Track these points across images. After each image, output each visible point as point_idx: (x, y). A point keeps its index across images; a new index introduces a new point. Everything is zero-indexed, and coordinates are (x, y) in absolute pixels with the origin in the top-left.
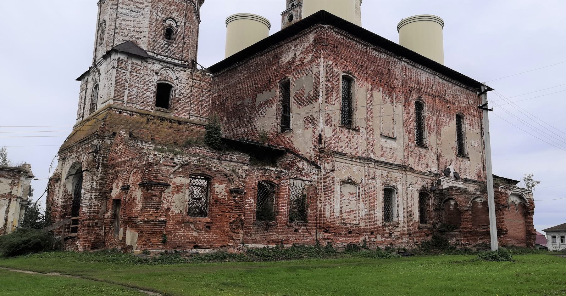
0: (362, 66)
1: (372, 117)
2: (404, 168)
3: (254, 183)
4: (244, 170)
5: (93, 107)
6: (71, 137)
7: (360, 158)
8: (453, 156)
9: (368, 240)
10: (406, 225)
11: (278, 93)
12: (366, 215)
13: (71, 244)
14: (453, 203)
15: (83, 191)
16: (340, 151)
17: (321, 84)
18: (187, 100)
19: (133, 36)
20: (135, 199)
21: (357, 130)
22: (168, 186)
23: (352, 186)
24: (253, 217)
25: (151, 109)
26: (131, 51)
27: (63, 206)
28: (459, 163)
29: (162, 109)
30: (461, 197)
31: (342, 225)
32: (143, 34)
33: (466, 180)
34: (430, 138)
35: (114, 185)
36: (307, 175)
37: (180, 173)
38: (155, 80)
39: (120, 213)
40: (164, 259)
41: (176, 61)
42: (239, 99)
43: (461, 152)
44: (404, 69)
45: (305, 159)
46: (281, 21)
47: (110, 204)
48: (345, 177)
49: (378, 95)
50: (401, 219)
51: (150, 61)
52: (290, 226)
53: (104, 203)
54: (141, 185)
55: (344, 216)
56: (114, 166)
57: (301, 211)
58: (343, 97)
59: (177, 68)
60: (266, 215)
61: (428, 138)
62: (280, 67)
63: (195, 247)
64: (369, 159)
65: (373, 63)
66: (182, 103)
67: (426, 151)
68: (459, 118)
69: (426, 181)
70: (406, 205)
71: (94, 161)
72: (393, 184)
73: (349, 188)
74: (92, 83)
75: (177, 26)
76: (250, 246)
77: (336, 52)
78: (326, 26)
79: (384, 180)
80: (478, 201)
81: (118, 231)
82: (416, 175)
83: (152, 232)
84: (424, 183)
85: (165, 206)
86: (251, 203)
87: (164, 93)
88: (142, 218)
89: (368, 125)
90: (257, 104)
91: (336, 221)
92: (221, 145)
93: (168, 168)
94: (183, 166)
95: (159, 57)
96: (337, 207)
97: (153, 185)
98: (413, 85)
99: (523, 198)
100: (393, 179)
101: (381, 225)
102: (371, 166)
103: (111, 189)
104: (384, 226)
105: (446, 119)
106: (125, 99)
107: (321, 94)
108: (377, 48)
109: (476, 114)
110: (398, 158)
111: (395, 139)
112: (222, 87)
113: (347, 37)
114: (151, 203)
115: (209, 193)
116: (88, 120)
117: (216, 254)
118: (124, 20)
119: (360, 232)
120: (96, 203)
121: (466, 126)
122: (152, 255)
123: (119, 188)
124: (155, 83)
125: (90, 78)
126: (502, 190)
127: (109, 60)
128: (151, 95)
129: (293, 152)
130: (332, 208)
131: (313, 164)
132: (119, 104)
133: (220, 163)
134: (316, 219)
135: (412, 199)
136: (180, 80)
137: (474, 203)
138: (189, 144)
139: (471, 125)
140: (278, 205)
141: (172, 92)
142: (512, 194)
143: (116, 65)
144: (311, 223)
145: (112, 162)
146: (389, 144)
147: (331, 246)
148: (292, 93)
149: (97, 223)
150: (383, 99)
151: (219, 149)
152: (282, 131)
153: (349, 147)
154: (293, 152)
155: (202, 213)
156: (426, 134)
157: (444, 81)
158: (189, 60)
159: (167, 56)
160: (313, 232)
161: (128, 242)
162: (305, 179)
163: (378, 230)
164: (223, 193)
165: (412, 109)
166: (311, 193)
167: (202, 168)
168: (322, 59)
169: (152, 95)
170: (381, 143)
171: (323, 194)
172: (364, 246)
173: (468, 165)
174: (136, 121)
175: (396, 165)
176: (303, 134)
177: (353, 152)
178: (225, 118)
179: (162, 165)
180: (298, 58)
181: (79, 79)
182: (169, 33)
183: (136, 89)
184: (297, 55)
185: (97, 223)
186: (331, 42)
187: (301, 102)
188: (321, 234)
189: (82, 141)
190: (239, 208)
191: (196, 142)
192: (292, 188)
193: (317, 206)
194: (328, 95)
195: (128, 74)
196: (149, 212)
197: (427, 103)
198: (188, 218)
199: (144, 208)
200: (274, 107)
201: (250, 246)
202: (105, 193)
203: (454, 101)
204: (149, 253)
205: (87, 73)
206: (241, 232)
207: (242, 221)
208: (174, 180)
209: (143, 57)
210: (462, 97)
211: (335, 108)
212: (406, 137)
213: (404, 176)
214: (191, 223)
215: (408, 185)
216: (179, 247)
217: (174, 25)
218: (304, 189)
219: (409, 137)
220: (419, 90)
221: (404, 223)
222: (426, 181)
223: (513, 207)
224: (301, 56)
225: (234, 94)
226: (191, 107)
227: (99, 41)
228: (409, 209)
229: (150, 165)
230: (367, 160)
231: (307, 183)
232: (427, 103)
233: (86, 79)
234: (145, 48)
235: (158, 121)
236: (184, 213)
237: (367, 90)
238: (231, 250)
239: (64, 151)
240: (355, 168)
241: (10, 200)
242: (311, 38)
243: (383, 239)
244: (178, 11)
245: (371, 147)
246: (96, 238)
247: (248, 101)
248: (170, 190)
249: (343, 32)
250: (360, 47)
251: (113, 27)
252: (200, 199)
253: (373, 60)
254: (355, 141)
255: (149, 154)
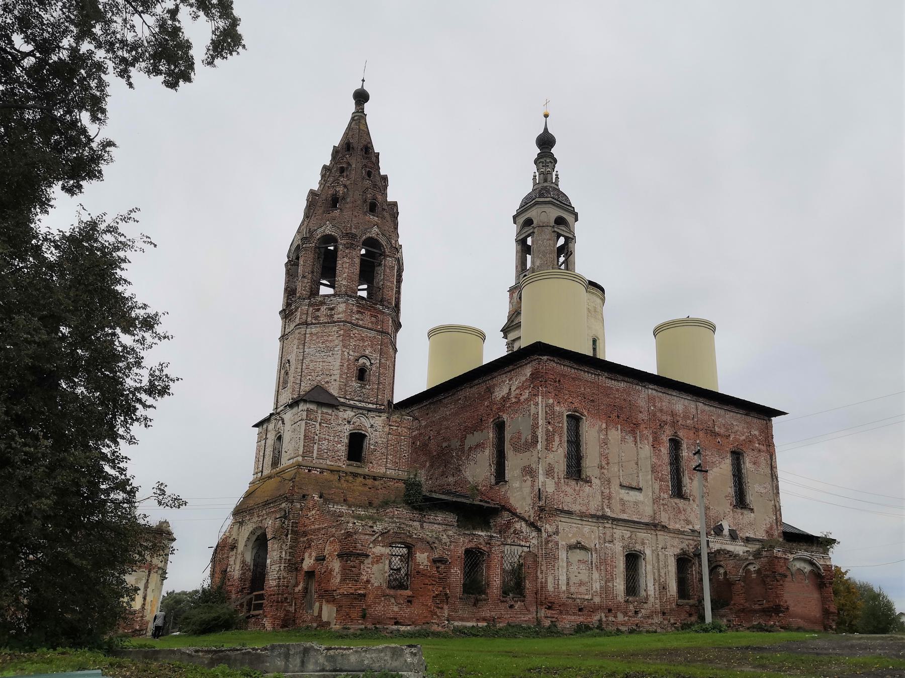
0: (593, 401)
1: (608, 464)
2: (655, 526)
3: (461, 551)
4: (448, 536)
5: (276, 462)
6: (249, 495)
7: (593, 516)
8: (728, 508)
9: (604, 619)
10: (657, 601)
11: (491, 435)
12: (601, 587)
13: (255, 623)
14: (722, 571)
15: (268, 561)
16: (566, 509)
17: (540, 428)
18: (384, 450)
19: (321, 380)
20: (331, 570)
21: (588, 481)
22: (367, 556)
23: (583, 552)
24: (459, 590)
25: (343, 464)
26: (319, 398)
27: (241, 579)
28: (737, 516)
29: (355, 463)
30: (731, 563)
31: (570, 601)
32: (333, 378)
33: (748, 540)
34: (692, 484)
35: (307, 555)
36: (526, 539)
37: (379, 542)
38: (347, 429)
39: (313, 587)
40: (364, 635)
41: (370, 406)
42: (445, 439)
43: (741, 501)
44: (651, 399)
45: (523, 519)
46: (508, 300)
47: (301, 577)
48: (573, 541)
49: (615, 434)
50: (651, 591)
51: (341, 408)
52: (503, 602)
53: (294, 576)
54: (339, 556)
55: (573, 589)
56: (305, 534)
57: (516, 584)
58: (568, 441)
59: (371, 414)
60: (474, 588)
61: (689, 485)
62: (492, 403)
63: (396, 623)
64: (604, 517)
65: (608, 395)
66: (378, 454)
67: (687, 502)
68: (737, 456)
69: (687, 542)
70: (659, 573)
71: (282, 527)
72: (638, 547)
73: (579, 555)
74: (274, 433)
75: (371, 364)
76: (456, 623)
77: (558, 387)
78: (545, 358)
79: (626, 543)
80: (751, 568)
81: (311, 608)
82: (672, 535)
83: (351, 606)
84: (684, 545)
85: (365, 578)
86: (457, 574)
87: (356, 444)
88: (341, 591)
89: (603, 473)
90: (466, 448)
91: (562, 595)
92: (421, 502)
93: (367, 537)
94: (382, 534)
95: (352, 402)
96: (563, 579)
97: (351, 555)
98: (664, 418)
99: (814, 564)
100: (639, 541)
101: (622, 601)
102: (607, 525)
103: (303, 559)
104: (627, 601)
105: (716, 459)
106: (315, 455)
107: (540, 440)
108: (612, 376)
109: (763, 448)
110: (646, 513)
111: (640, 489)
112: (424, 423)
113: (571, 367)
114: (350, 575)
115: (410, 563)
116: (270, 477)
117: (419, 631)
118: (312, 361)
119: (595, 609)
120: (285, 575)
121: (748, 465)
122: (352, 631)
123: (313, 558)
124: (347, 434)
125: (271, 426)
126: (780, 554)
127: (295, 410)
128: (342, 448)
129: (509, 510)
130: (556, 580)
131: (532, 525)
132: (308, 462)
133: (422, 527)
134: (536, 594)
135: (666, 566)
136: (376, 427)
137: (748, 572)
138: (386, 504)
139: (754, 464)
140: (488, 577)
141: (366, 441)
142: (794, 559)
143: (304, 417)
144: (530, 597)
145: (303, 529)
146: (633, 496)
147: (555, 626)
148: (508, 436)
149: (286, 599)
150: (623, 440)
151: (420, 509)
152: (497, 483)
153: (578, 502)
154: (509, 510)
155: (401, 586)
156: (686, 480)
157: (712, 408)
158: (386, 403)
159: (360, 401)
160: (533, 609)
161: (325, 618)
162: (523, 543)
163: (618, 607)
164: (426, 563)
165: (665, 450)
166: (530, 561)
167: (402, 536)
168: (540, 397)
169: (344, 448)
170: (621, 496)
171: (544, 563)
172: (600, 627)
173: (752, 519)
174: (326, 480)
175: (643, 523)
176: (521, 488)
177: (584, 509)
178: (428, 464)
179: (361, 533)
180: (513, 394)
181: (256, 426)
182: (362, 374)
183: (326, 443)
184: (513, 390)
185: (286, 599)
186: (551, 376)
187: (517, 449)
188: (543, 611)
189: (266, 504)
190: (443, 580)
191: (394, 502)
192: (506, 554)
193: (537, 577)
194: (549, 440)
195: (318, 425)
196: (348, 584)
197: (685, 440)
198: (388, 591)
199: (343, 580)
200: (487, 452)
201: (456, 623)
202: (294, 564)
203: (727, 434)
204: (349, 629)
205: (267, 420)
206: (446, 607)
207: (446, 594)
208: (373, 550)
209: (332, 404)
210: (739, 426)
211: (558, 456)
212: (657, 486)
213: (654, 537)
214: (392, 596)
215: (659, 549)
216: (379, 623)
217: (368, 364)
218: (520, 556)
219: (661, 486)
220: (674, 424)
221: (656, 598)
222: (687, 542)
223: (801, 577)
224: (517, 392)
225: (439, 433)
226: (387, 461)
227: (282, 383)
228: (662, 580)
229: (349, 535)
230: (601, 518)
231: (526, 549)
232: (685, 440)
233: (265, 426)
234: (335, 393)
235: (351, 478)
236: (384, 586)
237: (600, 430)
238: (435, 628)
239: (241, 512)
240: (586, 529)
241: (149, 572)
242: (528, 371)
243: (626, 618)
244: (372, 347)
245: (606, 501)
246: (286, 615)
247: (455, 443)
248: (369, 560)
249: (567, 363)
250: (587, 376)
251: (299, 370)
252: (399, 570)
253: (607, 392)
254: (585, 494)
255: (348, 523)
